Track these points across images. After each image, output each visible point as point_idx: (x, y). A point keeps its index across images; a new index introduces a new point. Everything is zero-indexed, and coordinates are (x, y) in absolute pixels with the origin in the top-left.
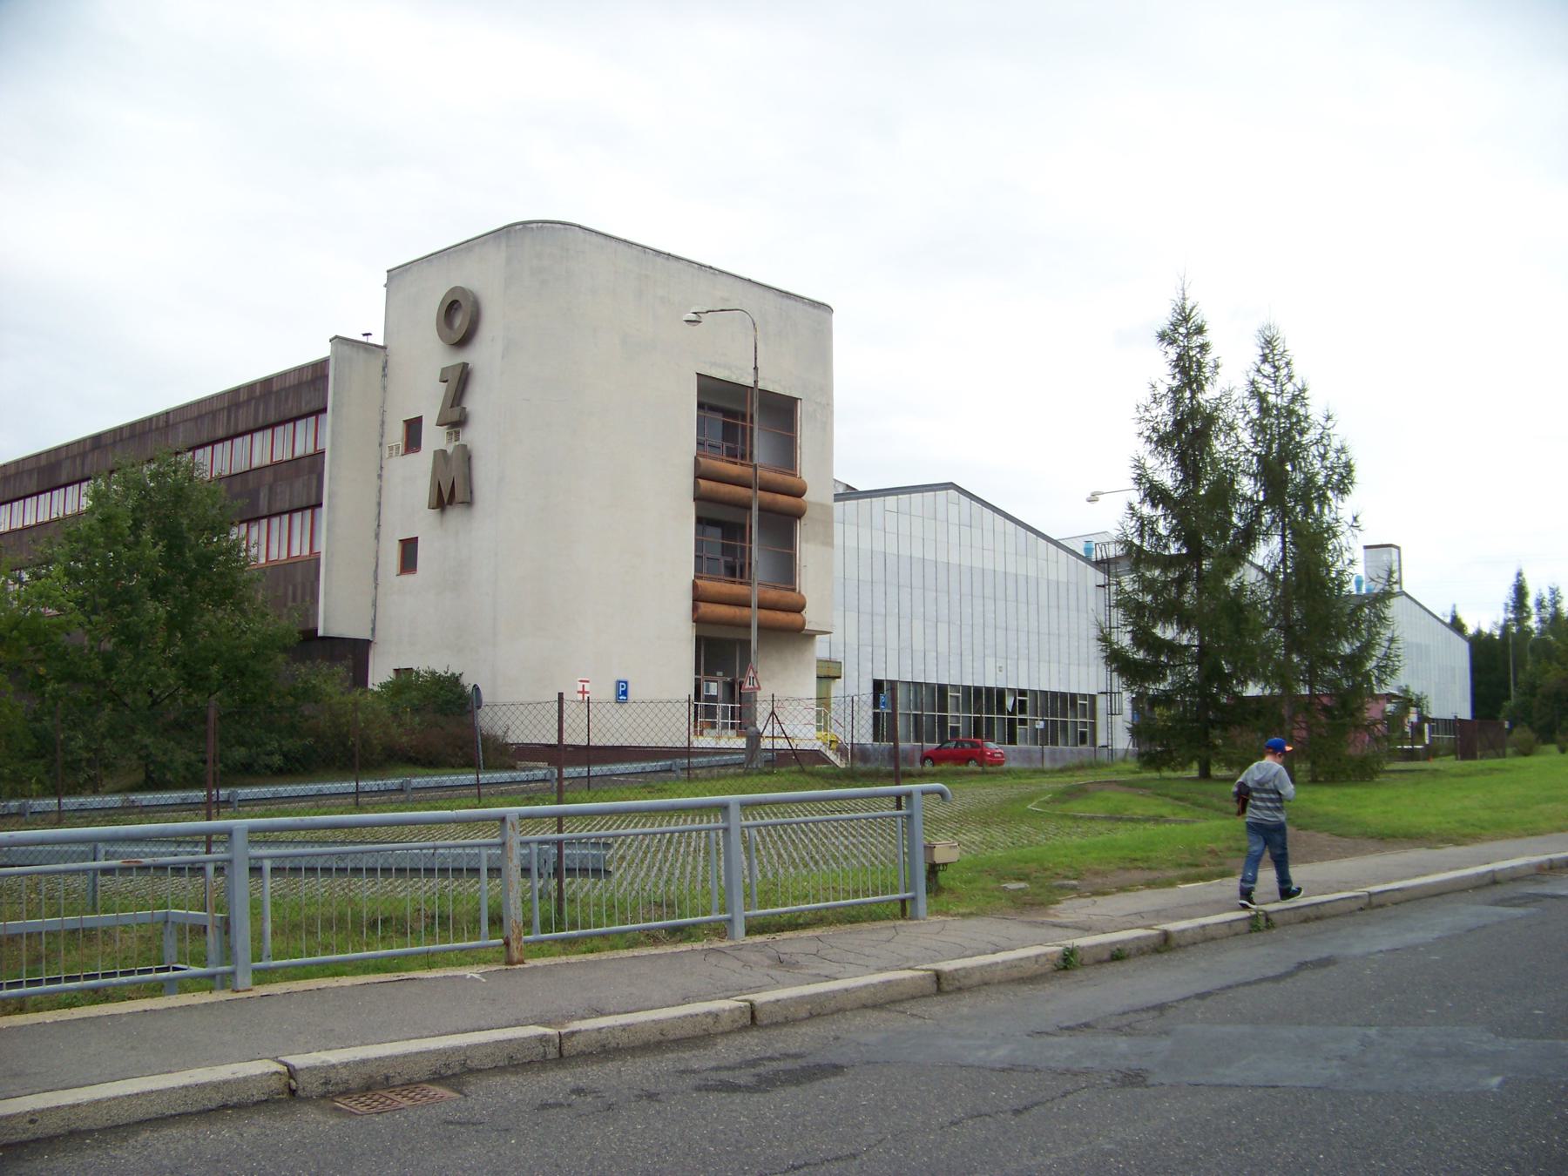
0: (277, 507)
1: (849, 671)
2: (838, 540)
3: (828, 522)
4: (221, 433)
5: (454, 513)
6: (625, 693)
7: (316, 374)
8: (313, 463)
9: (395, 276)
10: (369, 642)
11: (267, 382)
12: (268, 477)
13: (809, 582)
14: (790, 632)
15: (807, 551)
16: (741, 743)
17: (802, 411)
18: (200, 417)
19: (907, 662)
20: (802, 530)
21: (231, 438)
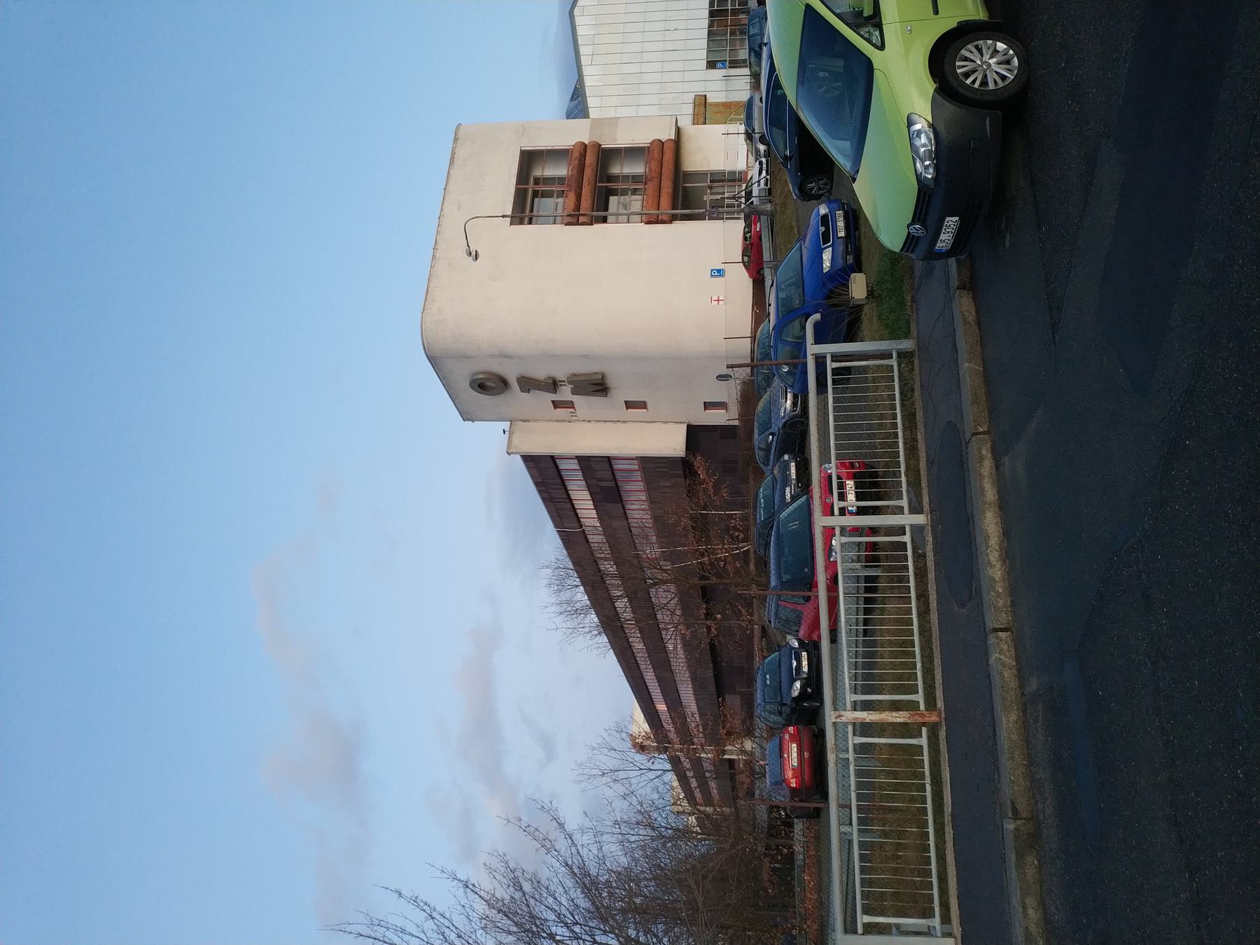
0: (610, 477)
1: (700, 89)
2: (611, 114)
3: (599, 122)
4: (569, 506)
5: (611, 382)
6: (719, 271)
7: (529, 460)
8: (586, 463)
9: (466, 416)
10: (689, 426)
11: (537, 484)
12: (594, 482)
13: (643, 137)
14: (671, 151)
15: (622, 138)
16: (799, 826)
17: (530, 146)
18: (559, 516)
19: (691, 55)
20: (607, 144)
21: (571, 500)
